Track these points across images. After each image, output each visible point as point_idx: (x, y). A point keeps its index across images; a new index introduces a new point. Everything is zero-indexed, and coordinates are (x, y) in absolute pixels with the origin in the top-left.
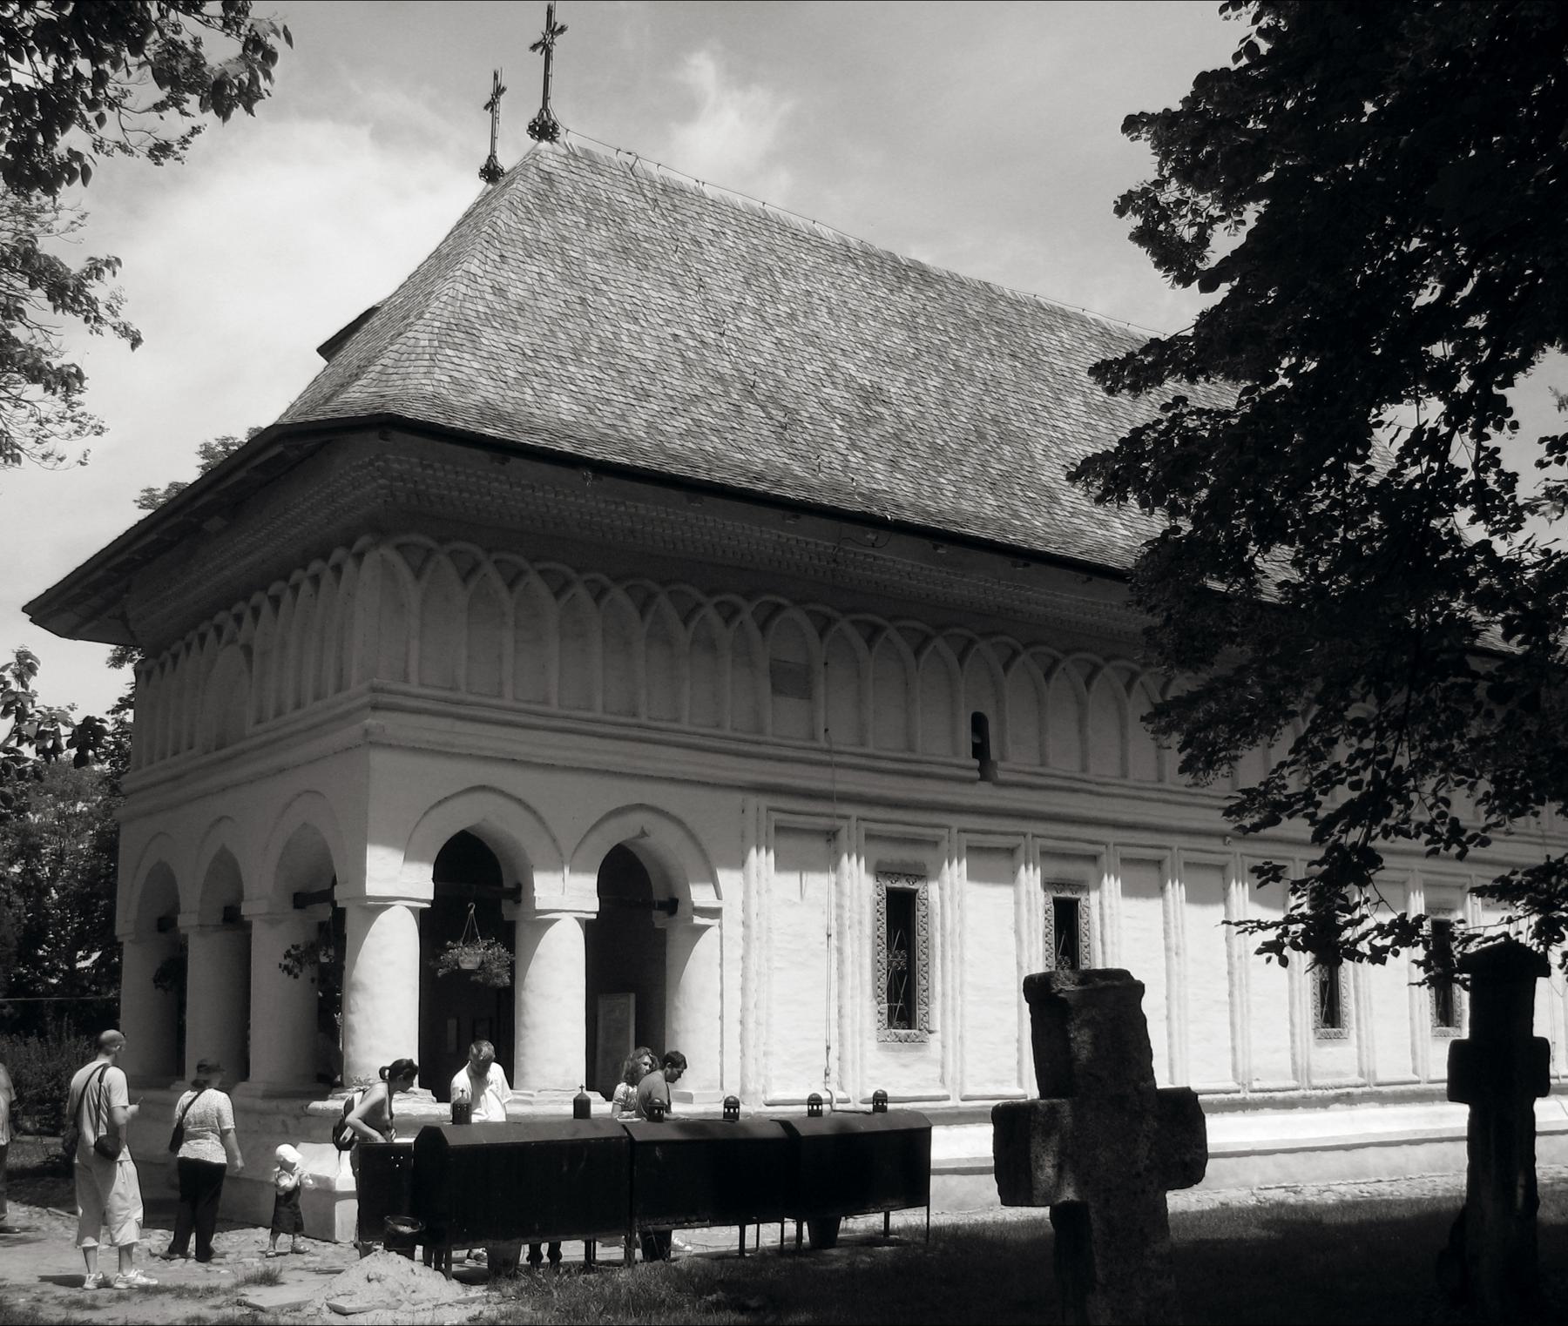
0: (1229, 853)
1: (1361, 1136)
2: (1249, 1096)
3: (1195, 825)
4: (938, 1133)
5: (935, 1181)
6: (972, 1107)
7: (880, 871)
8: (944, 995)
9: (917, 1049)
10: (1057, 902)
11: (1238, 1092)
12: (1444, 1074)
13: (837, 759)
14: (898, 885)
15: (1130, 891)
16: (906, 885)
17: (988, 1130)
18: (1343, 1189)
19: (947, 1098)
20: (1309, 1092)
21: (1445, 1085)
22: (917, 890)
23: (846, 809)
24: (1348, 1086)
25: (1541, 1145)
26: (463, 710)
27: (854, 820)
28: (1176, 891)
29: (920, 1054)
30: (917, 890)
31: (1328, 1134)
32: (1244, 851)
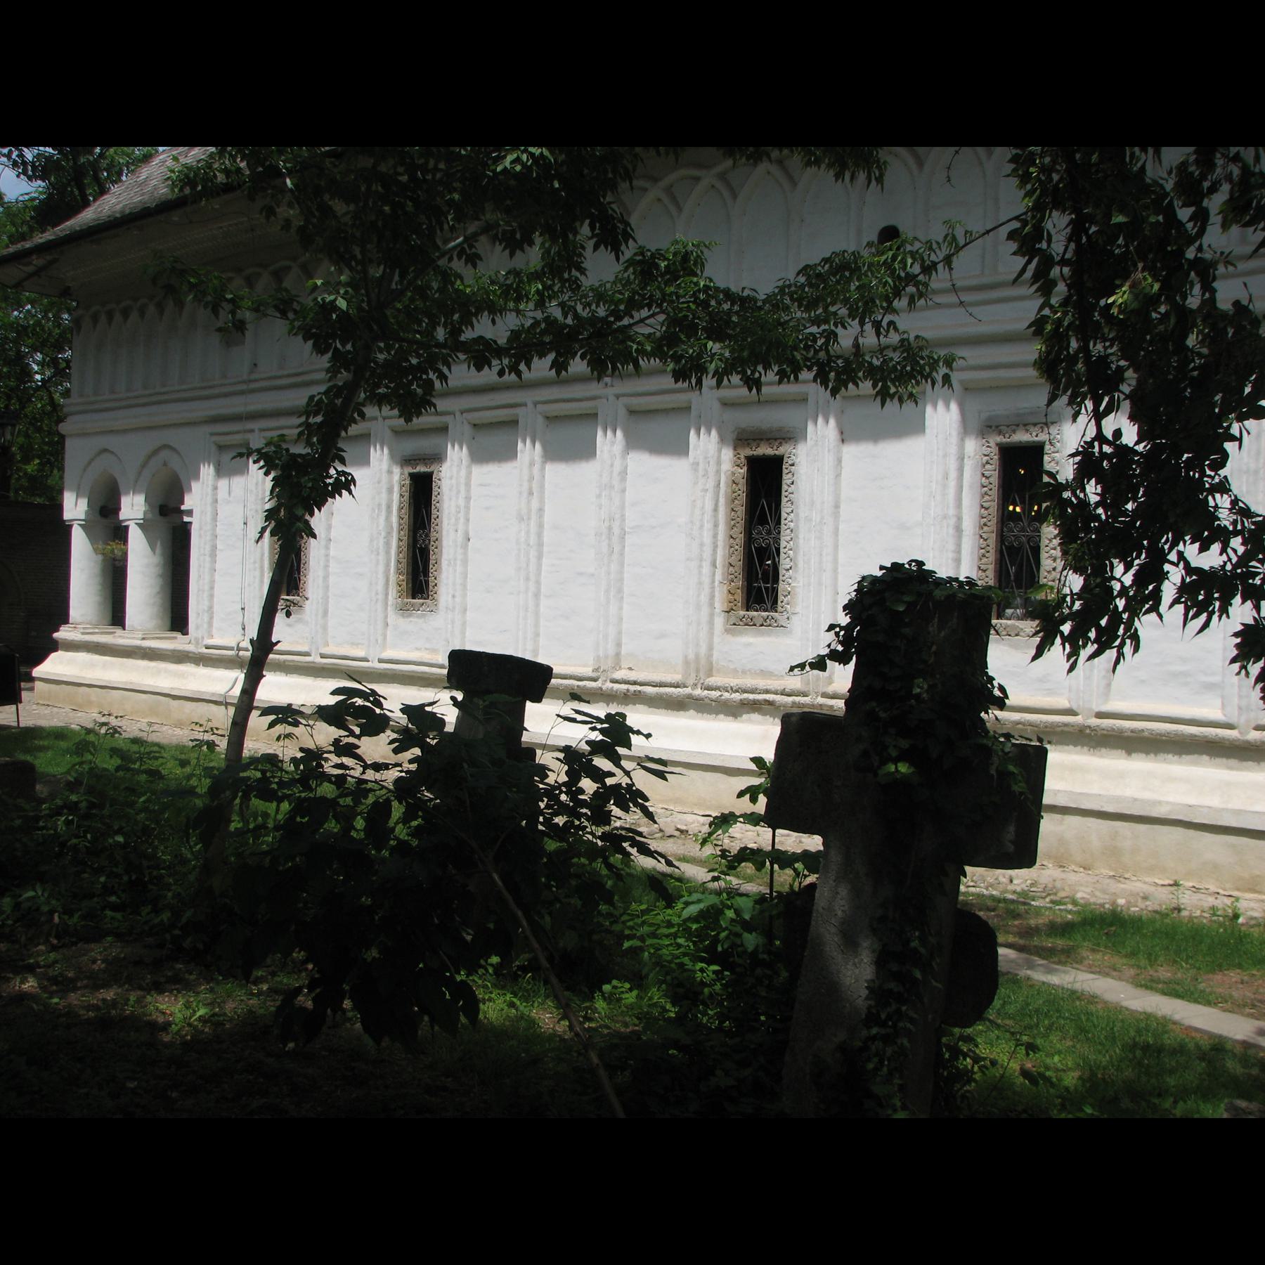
1: (1238, 812)
4: (1055, 757)
5: (1048, 826)
6: (413, 672)
7: (742, 439)
8: (714, 565)
10: (412, 476)
11: (595, 680)
13: (253, 386)
15: (480, 456)
17: (773, 730)
19: (307, 654)
20: (698, 692)
21: (445, 671)
23: (250, 425)
24: (767, 692)
26: (96, 406)
27: (530, 405)
28: (529, 451)
31: (1215, 801)
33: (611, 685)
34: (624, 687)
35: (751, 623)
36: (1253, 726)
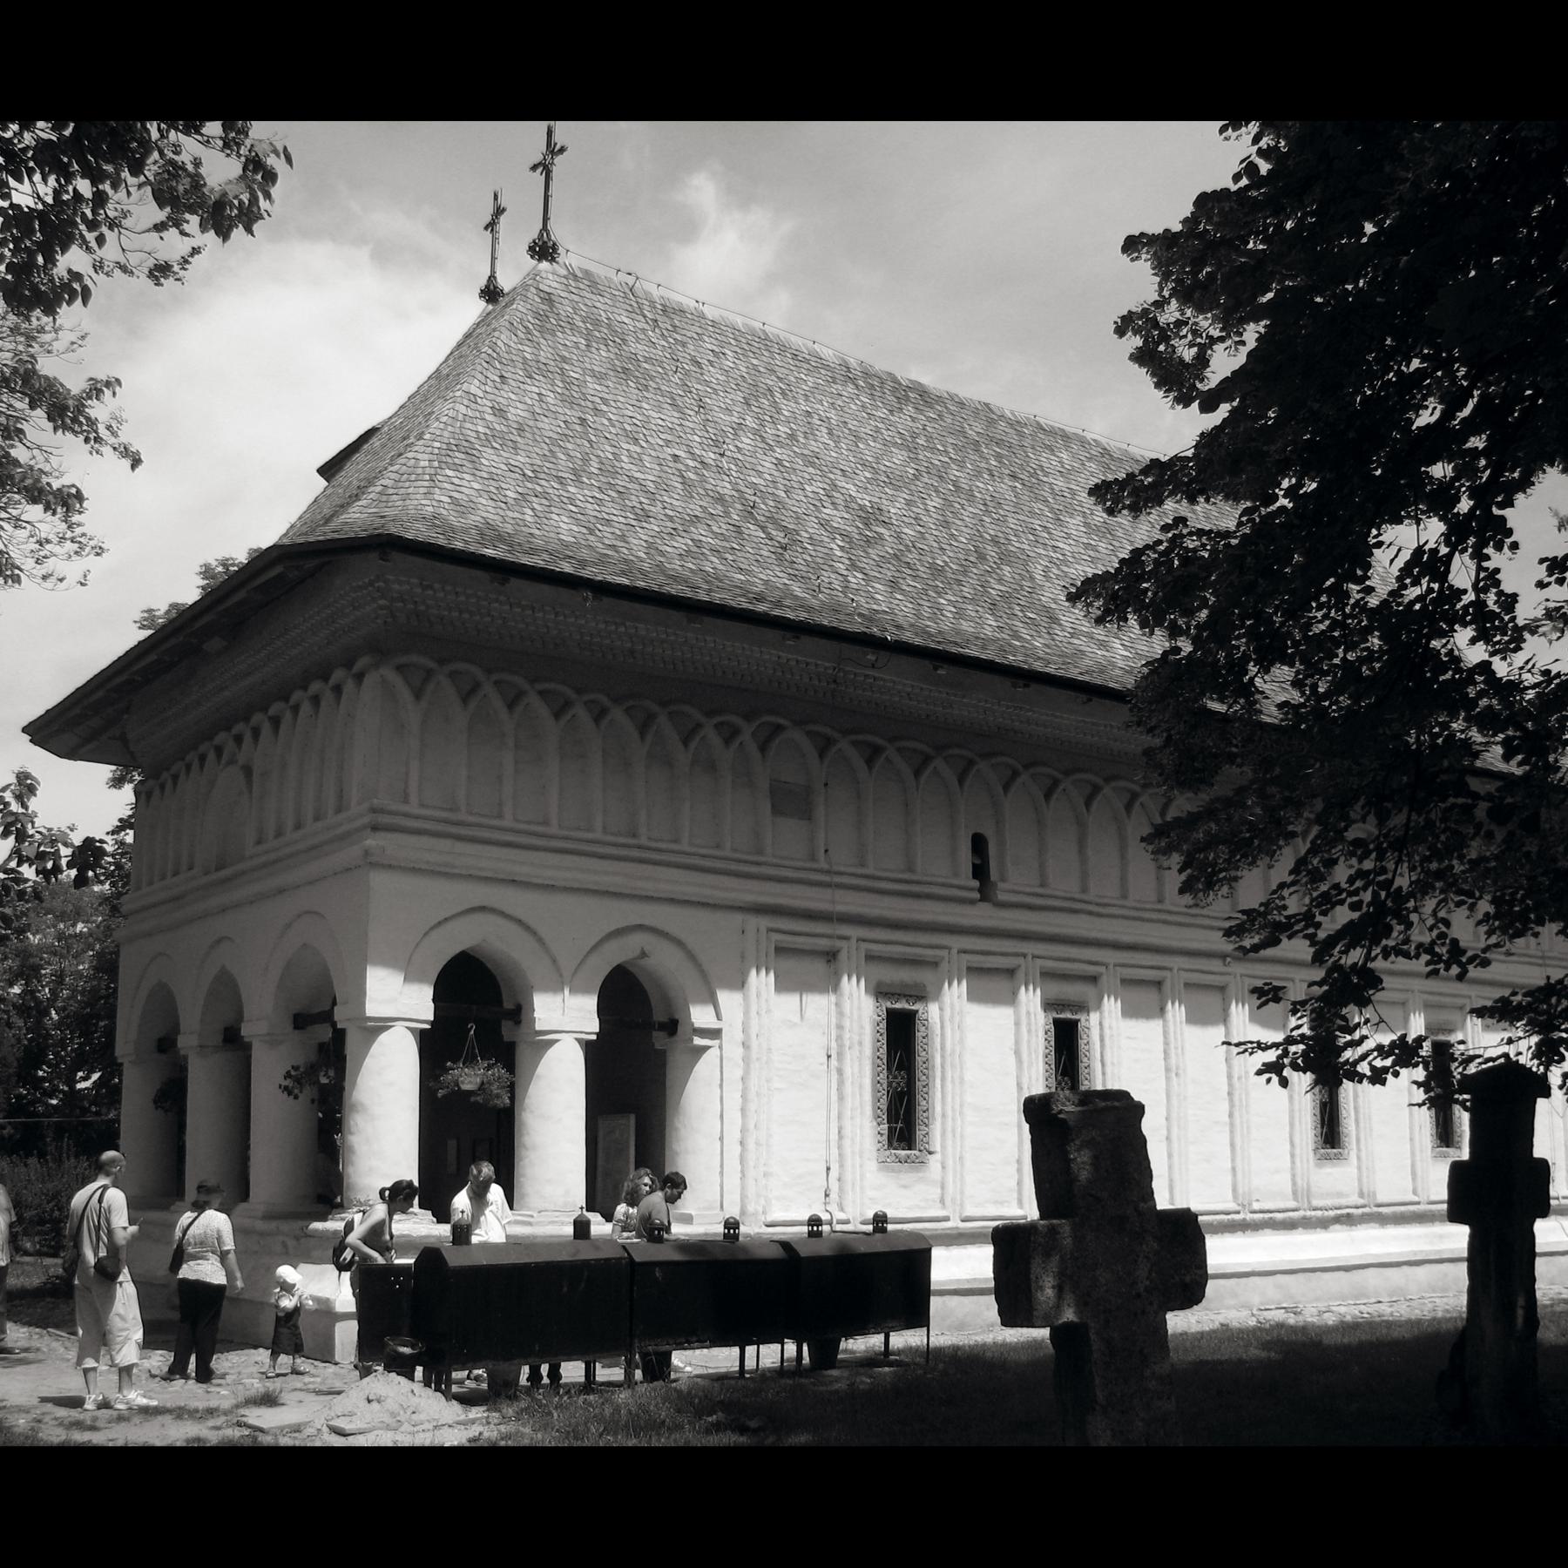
0: (1229, 974)
2: (1249, 1217)
3: (1195, 945)
4: (938, 1254)
9: (918, 1170)
10: (1057, 1022)
11: (1238, 1212)
12: (1444, 1195)
13: (837, 879)
14: (898, 1006)
15: (1130, 1012)
16: (907, 1006)
17: (988, 1251)
18: (1343, 1310)
19: (947, 1219)
20: (1309, 1213)
21: (1445, 1206)
22: (917, 1011)
24: (1348, 1207)
25: (1541, 1265)
26: (463, 831)
27: (854, 941)
29: (920, 1175)
30: (917, 1011)
32: (1244, 972)
33: (1252, 1215)
34: (1261, 1216)
35: (1328, 1158)
36: (860, 1220)
